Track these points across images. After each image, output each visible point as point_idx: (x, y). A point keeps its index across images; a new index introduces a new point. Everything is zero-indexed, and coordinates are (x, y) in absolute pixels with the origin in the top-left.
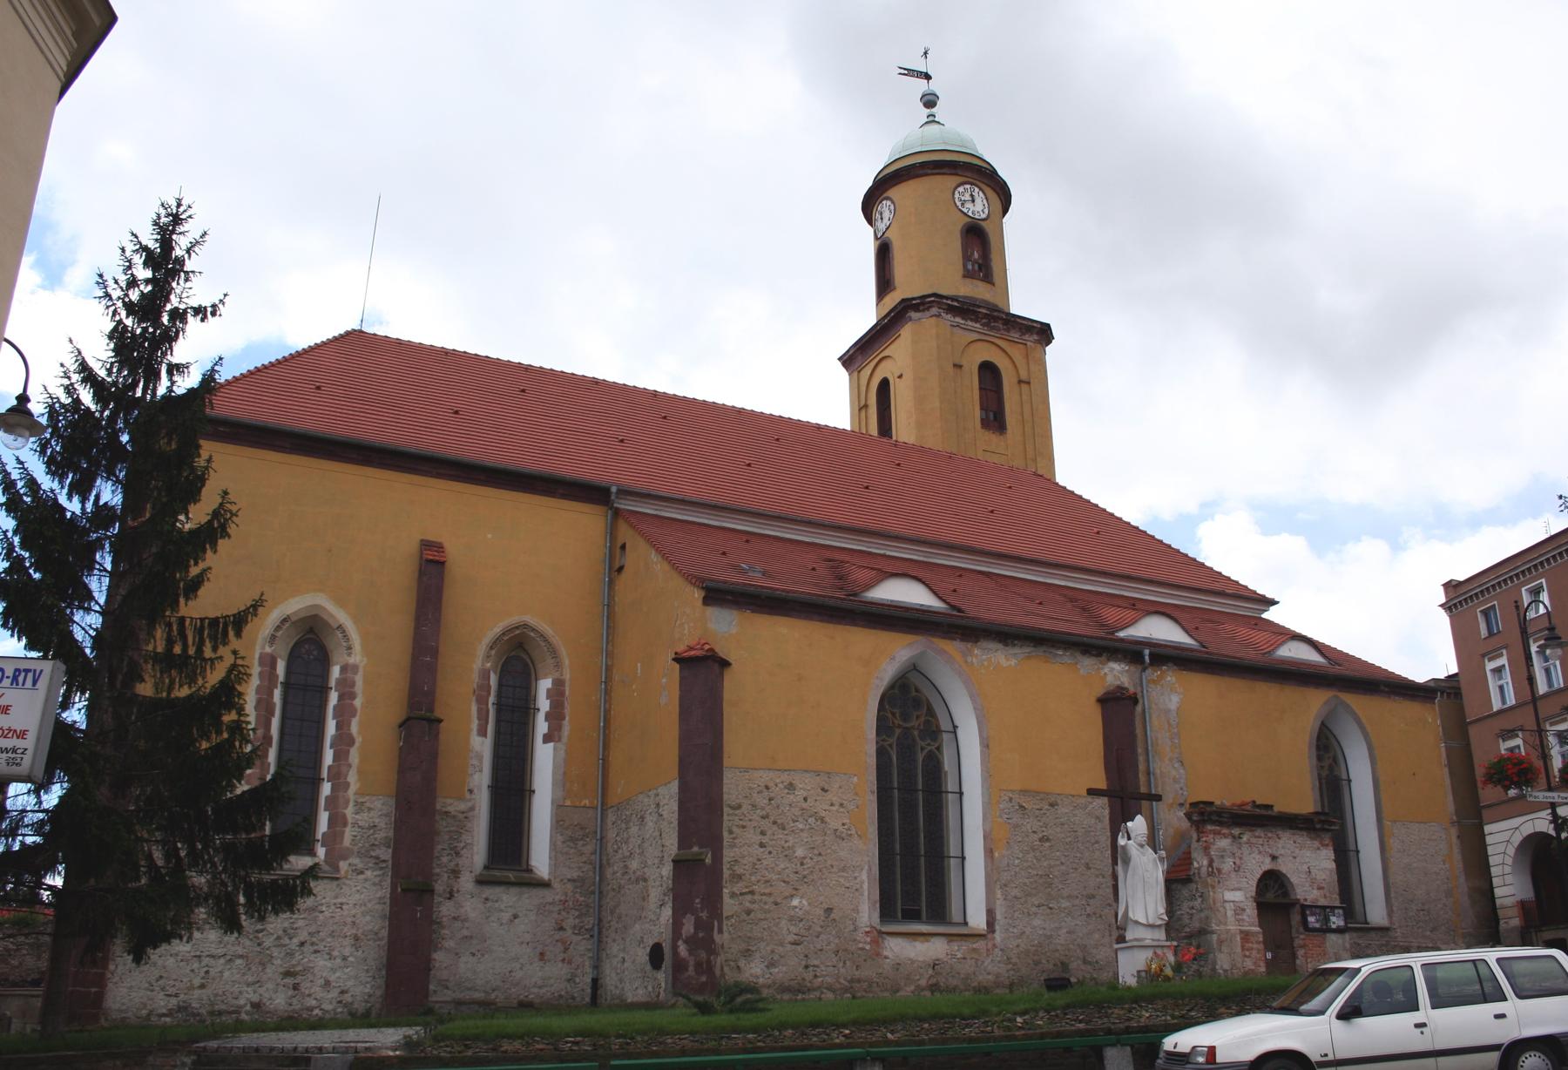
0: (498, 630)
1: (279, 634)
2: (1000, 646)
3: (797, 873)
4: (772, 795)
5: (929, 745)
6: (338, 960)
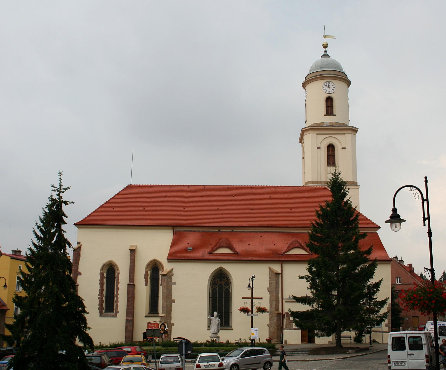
1: (103, 268)
5: (227, 287)
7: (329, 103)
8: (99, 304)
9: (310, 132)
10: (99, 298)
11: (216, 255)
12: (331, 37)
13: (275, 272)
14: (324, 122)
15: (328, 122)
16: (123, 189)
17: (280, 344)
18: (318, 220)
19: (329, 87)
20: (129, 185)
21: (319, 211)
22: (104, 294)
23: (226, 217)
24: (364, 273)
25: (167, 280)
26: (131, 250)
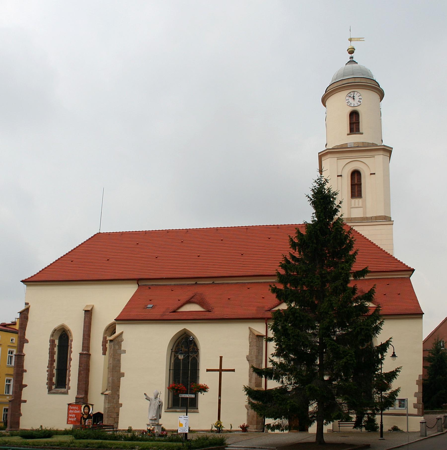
1: (54, 334)
5: (193, 355)
7: (354, 118)
8: (48, 378)
9: (329, 156)
10: (47, 371)
11: (181, 313)
12: (359, 39)
13: (256, 335)
14: (347, 144)
15: (352, 142)
16: (89, 239)
17: (261, 432)
18: (292, 251)
19: (354, 99)
20: (97, 233)
21: (294, 239)
22: (54, 365)
23: (201, 265)
24: (356, 329)
25: (114, 347)
26: (86, 311)
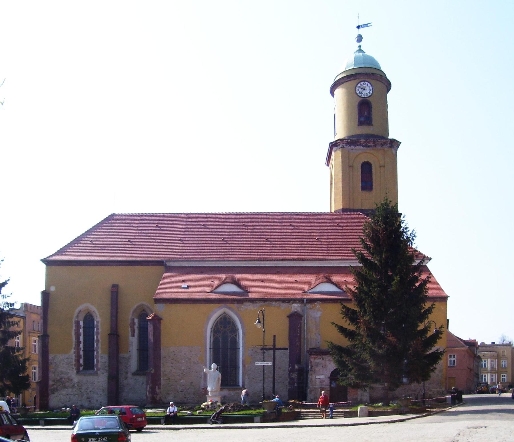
0: (135, 307)
2: (251, 304)
3: (182, 373)
4: (175, 353)
5: (233, 335)
6: (99, 395)
